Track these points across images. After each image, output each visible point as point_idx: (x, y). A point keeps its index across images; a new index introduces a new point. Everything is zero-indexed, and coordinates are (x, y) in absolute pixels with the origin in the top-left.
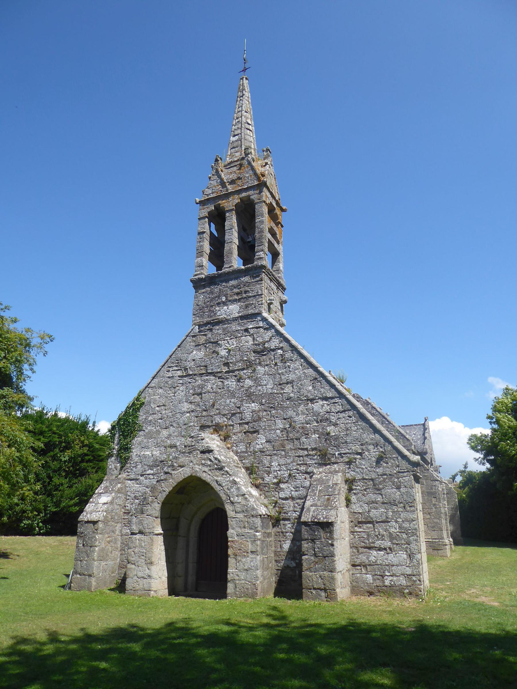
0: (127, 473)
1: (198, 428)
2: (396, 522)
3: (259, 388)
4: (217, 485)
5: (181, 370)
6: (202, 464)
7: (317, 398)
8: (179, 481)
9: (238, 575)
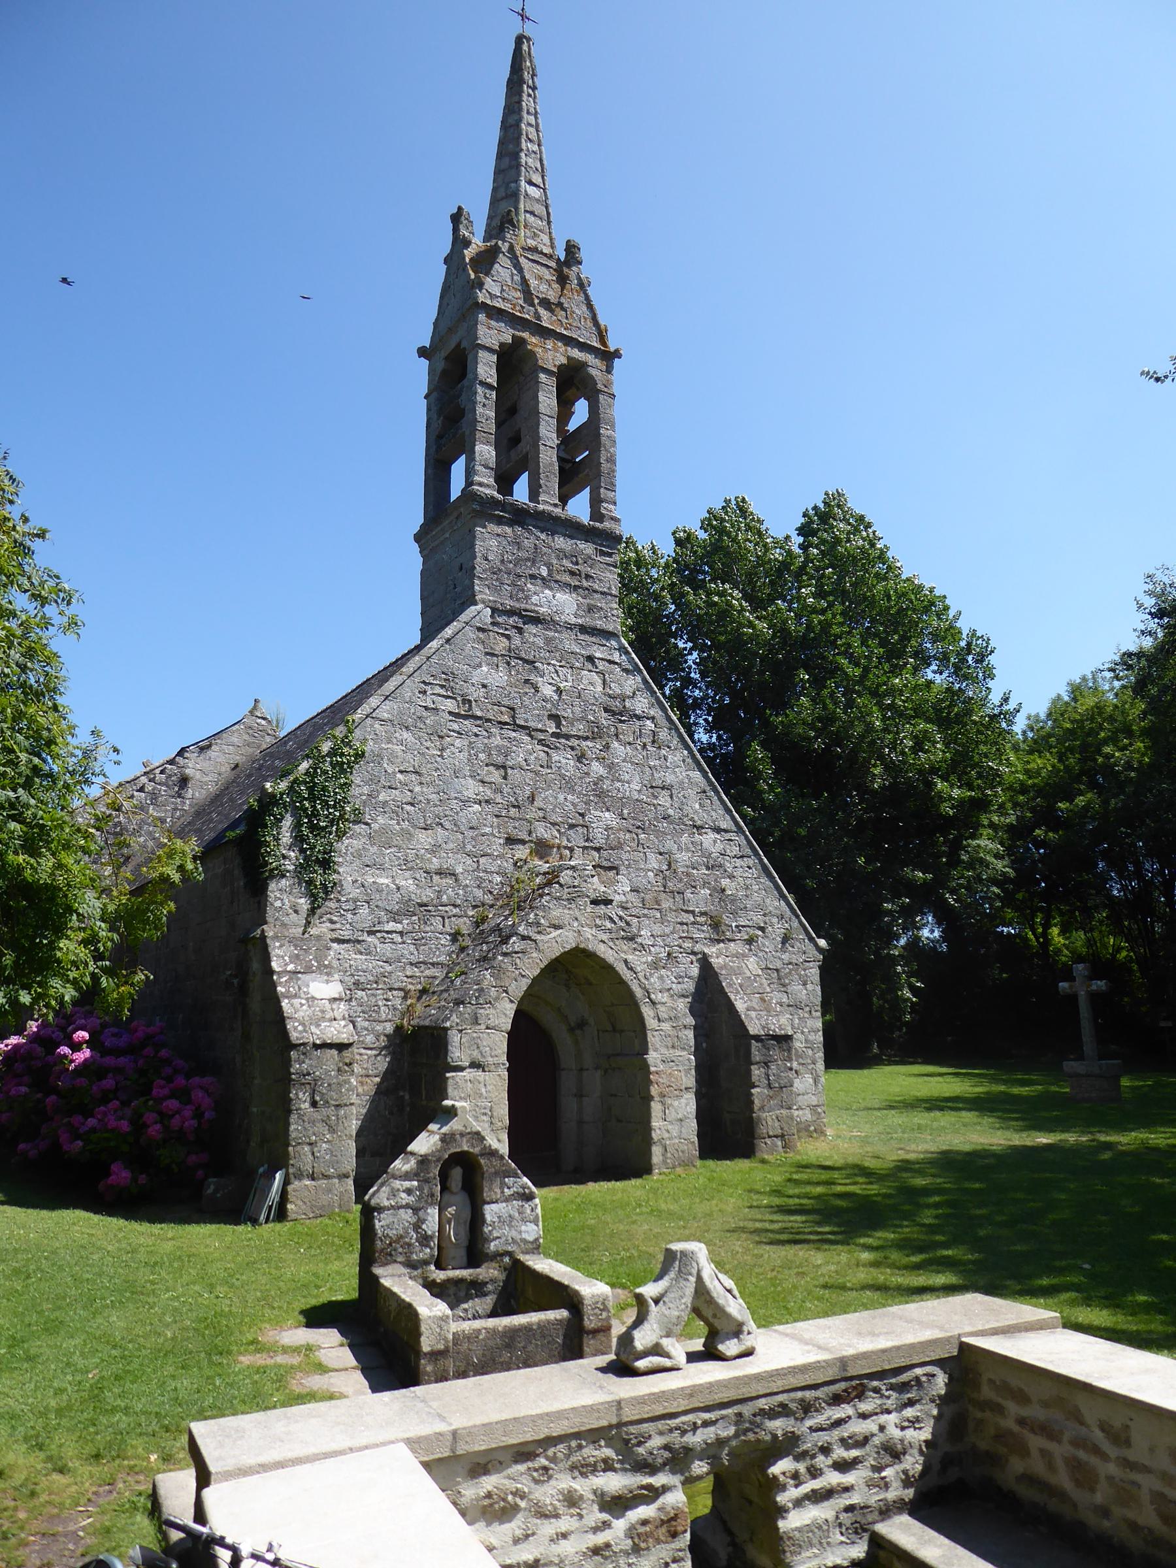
0: (329, 925)
1: (502, 841)
2: (803, 1033)
3: (618, 784)
6: (597, 926)
8: (554, 957)
9: (668, 1131)
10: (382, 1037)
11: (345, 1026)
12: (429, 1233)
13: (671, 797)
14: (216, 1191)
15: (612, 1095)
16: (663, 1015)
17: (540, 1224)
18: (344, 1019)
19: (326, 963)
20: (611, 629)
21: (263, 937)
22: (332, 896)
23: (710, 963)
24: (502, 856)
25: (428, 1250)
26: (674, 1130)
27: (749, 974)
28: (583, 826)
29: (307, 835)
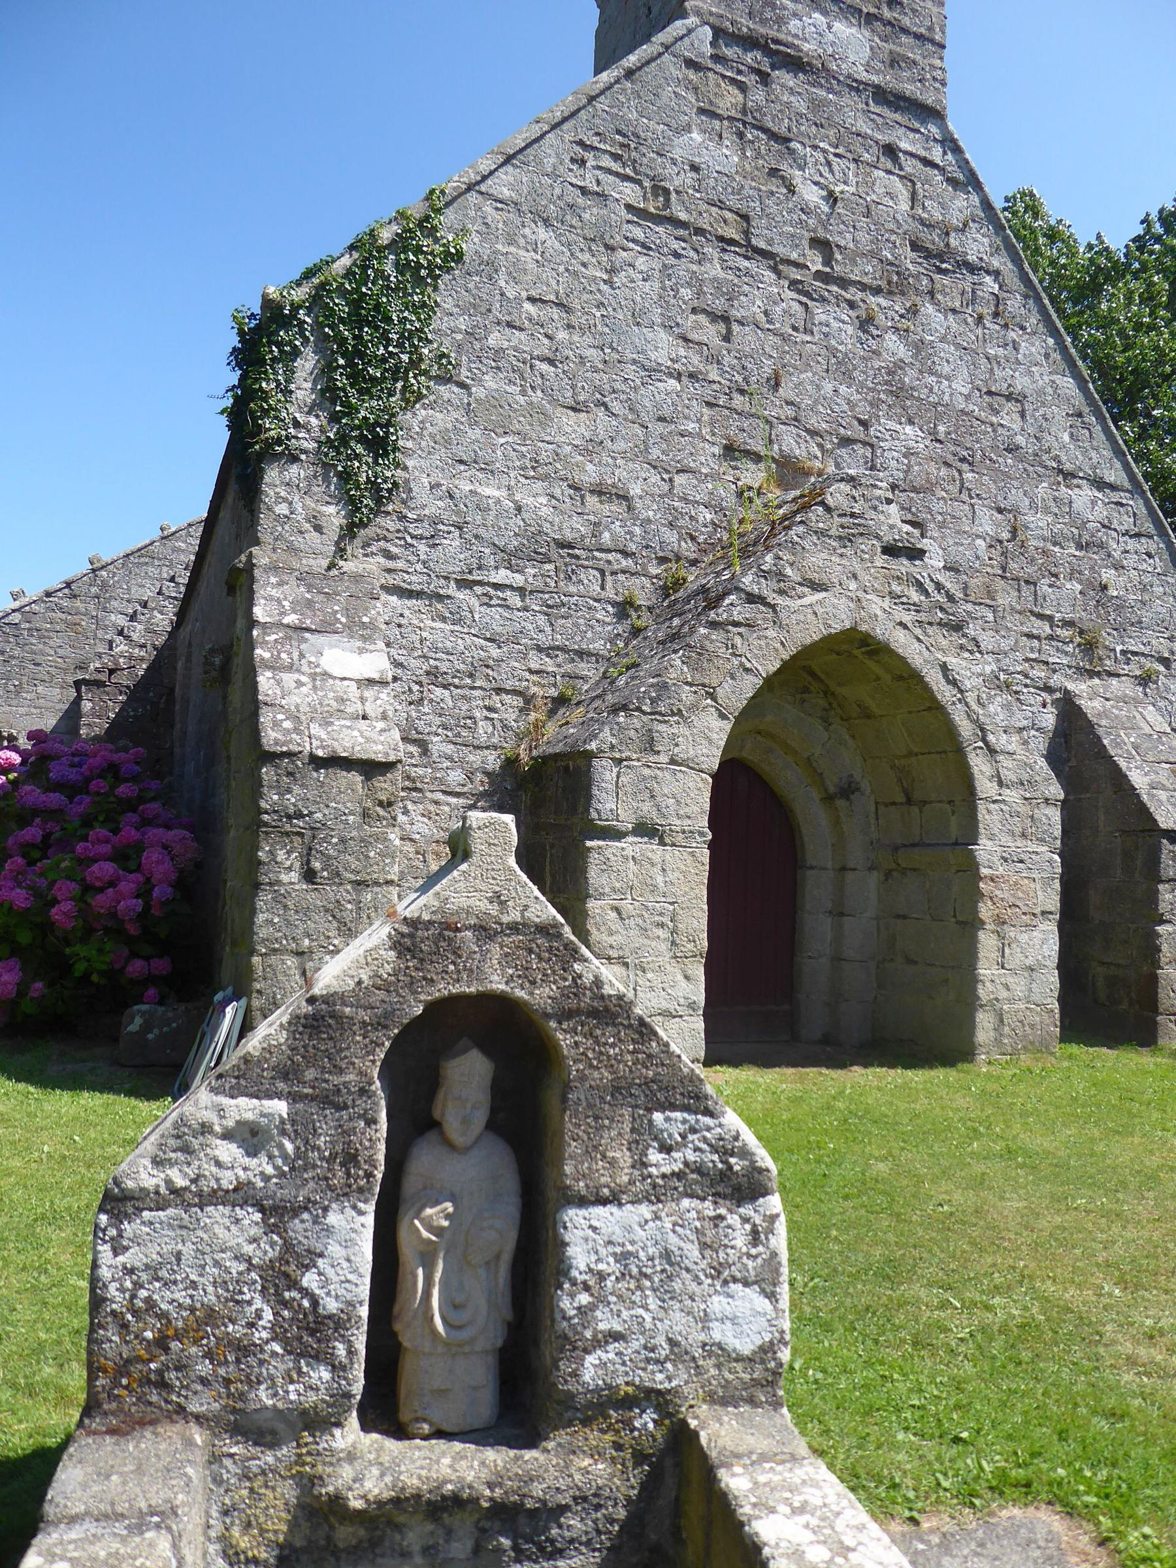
0: (382, 560)
1: (716, 450)
3: (931, 380)
4: (943, 681)
5: (639, 182)
7: (1081, 475)
8: (808, 641)
10: (479, 776)
11: (383, 731)
12: (331, 1306)
13: (1023, 414)
14: (147, 1027)
15: (898, 916)
16: (1008, 776)
17: (784, 1290)
18: (384, 717)
19: (365, 619)
20: (929, 101)
21: (250, 566)
22: (390, 508)
23: (1079, 708)
24: (714, 476)
25: (326, 1375)
26: (1019, 986)
27: (1148, 730)
28: (865, 444)
29: (344, 390)
